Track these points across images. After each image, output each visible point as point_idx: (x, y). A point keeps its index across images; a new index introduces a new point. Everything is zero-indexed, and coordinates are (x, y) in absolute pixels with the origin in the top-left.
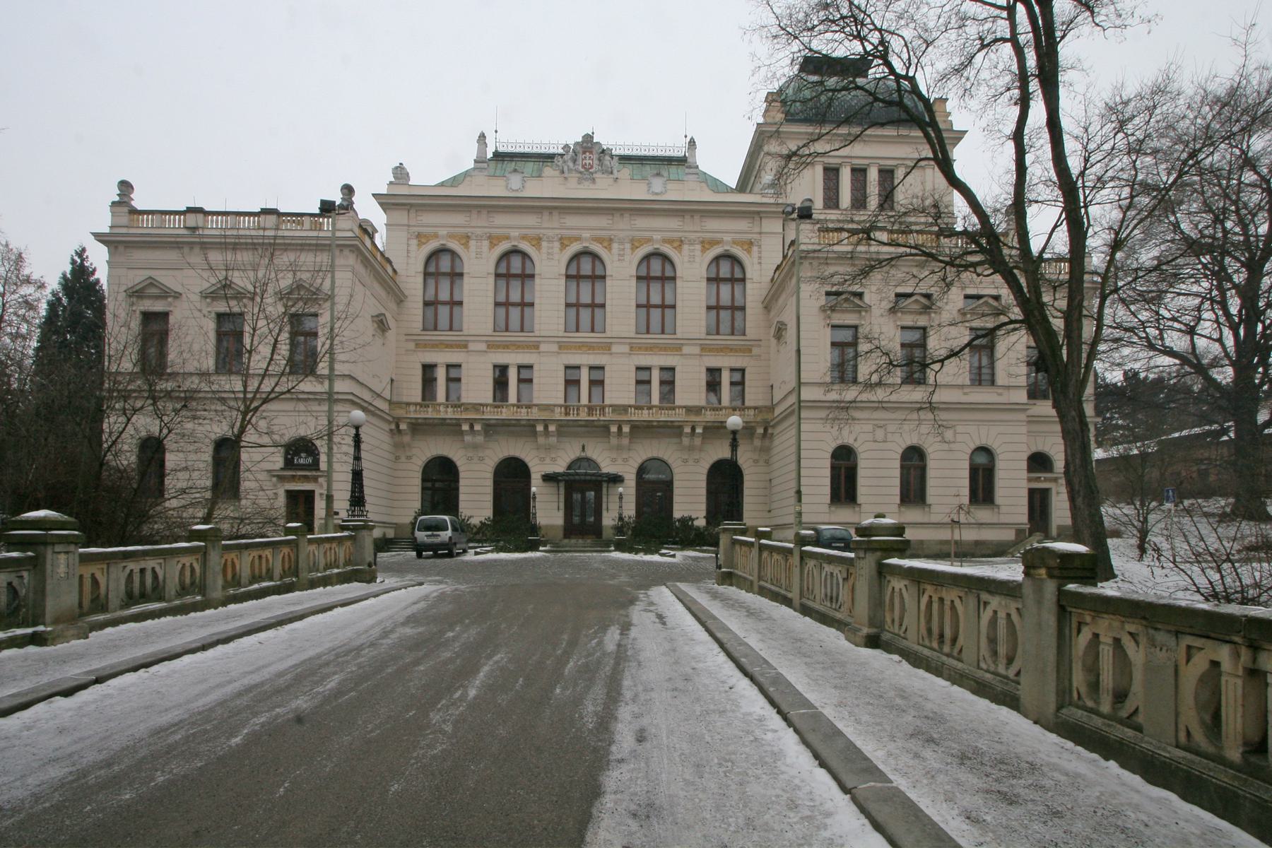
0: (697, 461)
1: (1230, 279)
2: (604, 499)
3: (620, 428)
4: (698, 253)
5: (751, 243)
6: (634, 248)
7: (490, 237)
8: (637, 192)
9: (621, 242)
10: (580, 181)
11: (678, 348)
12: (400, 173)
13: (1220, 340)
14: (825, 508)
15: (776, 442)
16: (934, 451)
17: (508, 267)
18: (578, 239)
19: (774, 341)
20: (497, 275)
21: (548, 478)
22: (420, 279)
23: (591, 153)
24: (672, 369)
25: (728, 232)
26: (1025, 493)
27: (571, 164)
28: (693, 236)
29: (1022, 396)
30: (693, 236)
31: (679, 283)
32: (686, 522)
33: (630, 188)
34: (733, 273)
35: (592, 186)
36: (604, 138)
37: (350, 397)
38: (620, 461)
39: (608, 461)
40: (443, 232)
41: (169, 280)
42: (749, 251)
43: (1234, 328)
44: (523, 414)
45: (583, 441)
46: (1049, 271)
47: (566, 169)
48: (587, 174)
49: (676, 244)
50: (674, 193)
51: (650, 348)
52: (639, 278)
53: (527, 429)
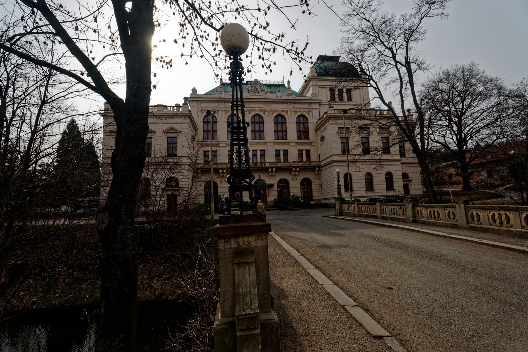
0: (297, 179)
1: (452, 121)
2: (267, 192)
3: (223, 171)
4: (293, 115)
5: (309, 112)
6: (272, 113)
8: (272, 96)
9: (268, 111)
11: (289, 144)
12: (194, 91)
13: (452, 138)
14: (385, 191)
15: (323, 172)
16: (374, 174)
17: (208, 119)
18: (254, 111)
19: (319, 142)
20: (204, 122)
22: (202, 124)
24: (264, 151)
25: (302, 108)
26: (402, 185)
29: (398, 157)
30: (291, 109)
31: (265, 124)
34: (259, 120)
36: (259, 80)
39: (268, 180)
40: (280, 110)
41: (177, 127)
42: (309, 114)
43: (456, 135)
44: (286, 165)
45: (259, 174)
46: (400, 119)
48: (256, 91)
51: (280, 144)
52: (274, 122)
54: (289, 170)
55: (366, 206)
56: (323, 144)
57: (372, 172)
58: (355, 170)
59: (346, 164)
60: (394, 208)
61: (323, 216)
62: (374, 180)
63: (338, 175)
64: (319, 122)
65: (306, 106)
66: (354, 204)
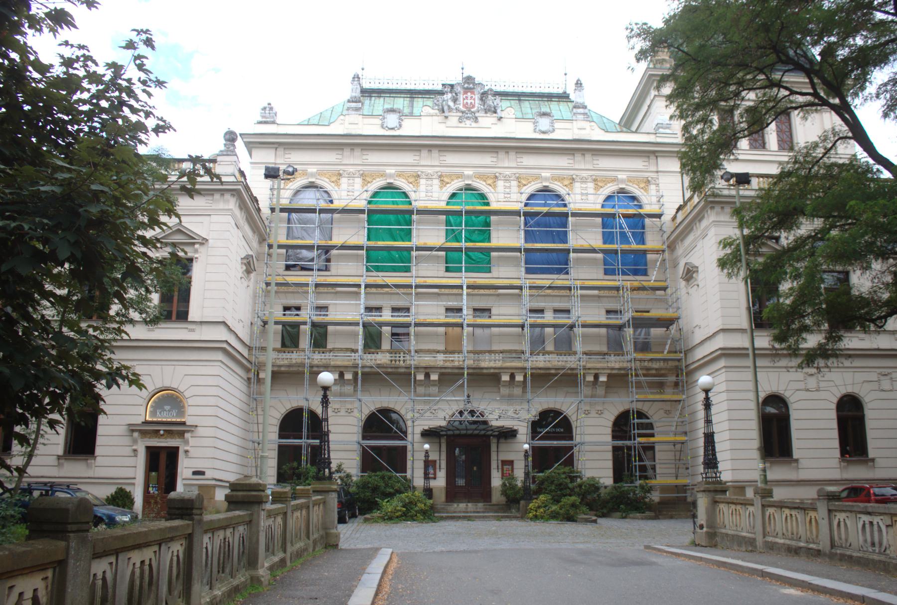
0: (600, 413)
5: (648, 182)
7: (363, 176)
9: (507, 179)
10: (460, 120)
21: (428, 434)
23: (473, 93)
27: (451, 104)
28: (584, 174)
30: (584, 174)
32: (594, 487)
33: (513, 124)
35: (474, 125)
37: (225, 345)
38: (593, 414)
42: (646, 190)
47: (446, 108)
49: (566, 182)
50: (564, 132)
53: (402, 377)
54: (568, 380)
55: (733, 507)
56: (693, 291)
57: (787, 394)
58: (875, 386)
59: (749, 362)
60: (871, 523)
61: (647, 547)
62: (794, 425)
63: (707, 399)
64: (680, 216)
65: (637, 164)
66: (815, 509)
